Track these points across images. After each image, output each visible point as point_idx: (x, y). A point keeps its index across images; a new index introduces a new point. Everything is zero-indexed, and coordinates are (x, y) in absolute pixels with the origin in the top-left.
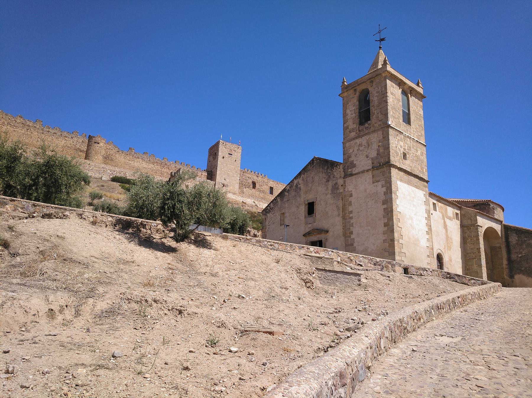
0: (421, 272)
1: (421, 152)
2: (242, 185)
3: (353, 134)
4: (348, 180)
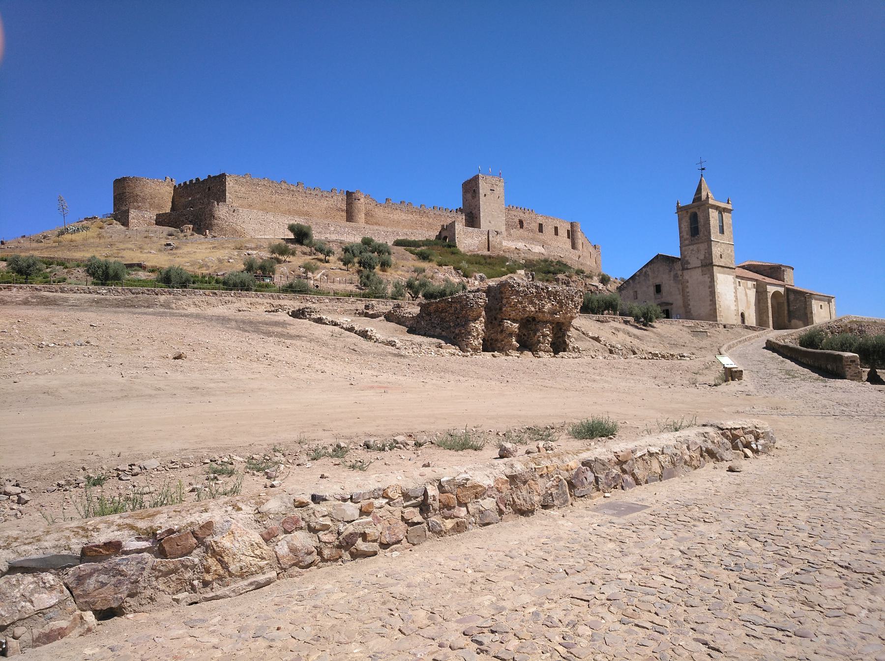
0: (732, 326)
1: (730, 251)
2: (509, 226)
3: (687, 242)
4: (685, 272)
